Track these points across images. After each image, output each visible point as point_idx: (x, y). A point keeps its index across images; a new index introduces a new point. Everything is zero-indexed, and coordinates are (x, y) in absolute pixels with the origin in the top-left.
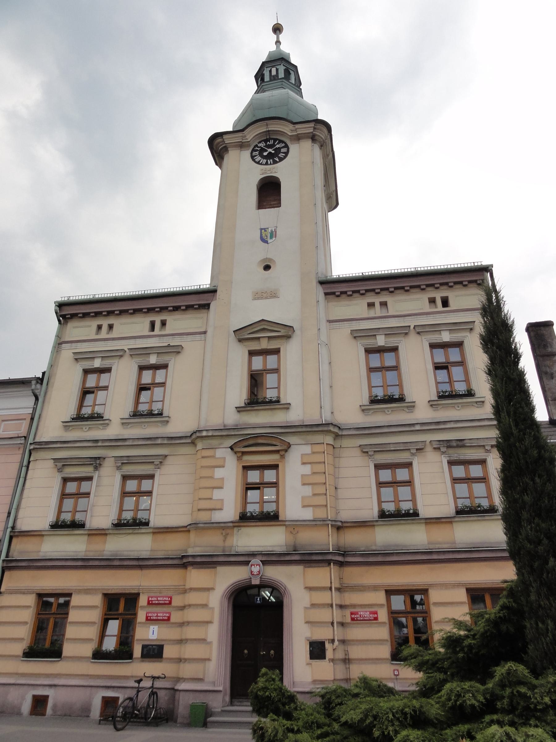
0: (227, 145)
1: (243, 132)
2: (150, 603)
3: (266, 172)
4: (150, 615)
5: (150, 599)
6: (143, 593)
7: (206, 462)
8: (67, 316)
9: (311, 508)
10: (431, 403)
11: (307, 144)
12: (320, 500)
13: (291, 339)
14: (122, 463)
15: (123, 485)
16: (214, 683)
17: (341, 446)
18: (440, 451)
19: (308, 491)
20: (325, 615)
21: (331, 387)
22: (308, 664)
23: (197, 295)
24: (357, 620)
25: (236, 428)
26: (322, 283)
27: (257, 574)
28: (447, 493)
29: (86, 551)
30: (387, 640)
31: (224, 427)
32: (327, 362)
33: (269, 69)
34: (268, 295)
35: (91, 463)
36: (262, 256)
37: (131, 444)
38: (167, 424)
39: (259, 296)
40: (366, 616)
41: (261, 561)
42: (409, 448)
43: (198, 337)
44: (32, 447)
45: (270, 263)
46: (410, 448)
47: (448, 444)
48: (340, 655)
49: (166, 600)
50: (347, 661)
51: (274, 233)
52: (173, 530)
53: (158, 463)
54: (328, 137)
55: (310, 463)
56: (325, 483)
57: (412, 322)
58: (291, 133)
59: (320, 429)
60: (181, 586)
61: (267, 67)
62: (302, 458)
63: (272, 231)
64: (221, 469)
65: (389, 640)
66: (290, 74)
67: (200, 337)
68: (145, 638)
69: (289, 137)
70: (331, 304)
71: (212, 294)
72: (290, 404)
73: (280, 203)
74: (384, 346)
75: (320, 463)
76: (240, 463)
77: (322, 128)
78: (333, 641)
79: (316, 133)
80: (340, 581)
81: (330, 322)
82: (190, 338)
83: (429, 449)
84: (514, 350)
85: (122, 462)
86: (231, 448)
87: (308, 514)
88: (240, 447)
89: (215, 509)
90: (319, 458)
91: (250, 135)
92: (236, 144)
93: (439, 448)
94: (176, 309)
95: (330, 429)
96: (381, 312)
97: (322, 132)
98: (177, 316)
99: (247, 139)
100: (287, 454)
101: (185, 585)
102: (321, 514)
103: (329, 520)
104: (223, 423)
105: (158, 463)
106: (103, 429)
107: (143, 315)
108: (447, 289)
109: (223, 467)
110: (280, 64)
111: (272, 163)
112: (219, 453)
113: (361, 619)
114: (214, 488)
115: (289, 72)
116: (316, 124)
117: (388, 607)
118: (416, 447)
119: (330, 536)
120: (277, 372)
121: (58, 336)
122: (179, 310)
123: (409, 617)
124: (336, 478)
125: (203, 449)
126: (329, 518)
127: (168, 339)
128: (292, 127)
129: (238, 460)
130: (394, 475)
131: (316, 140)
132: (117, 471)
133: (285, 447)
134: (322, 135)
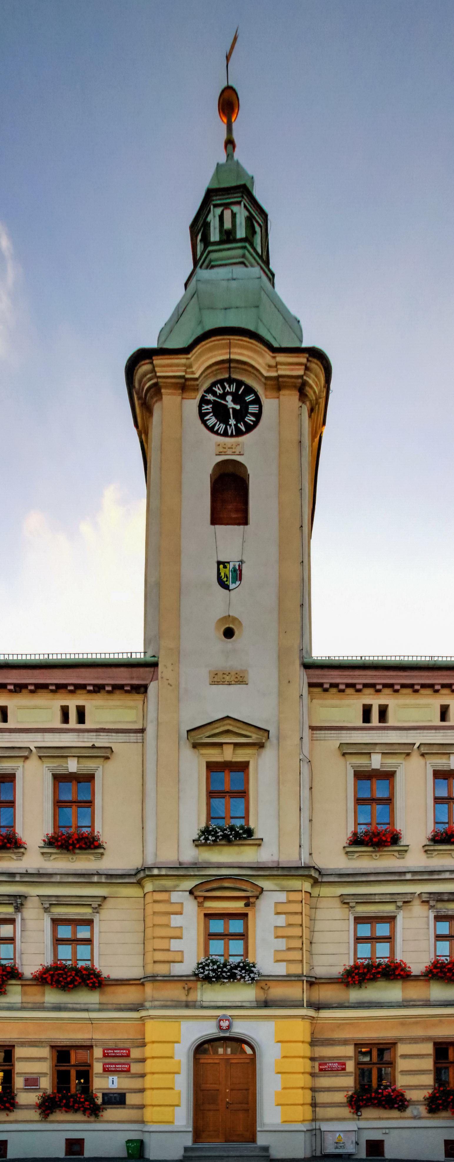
1: (189, 356)
2: (105, 1056)
3: (225, 450)
4: (107, 1066)
5: (106, 1051)
7: (159, 908)
9: (285, 964)
10: (427, 848)
14: (51, 904)
15: (54, 931)
17: (319, 895)
19: (282, 944)
21: (311, 820)
23: (130, 670)
24: (325, 1070)
25: (196, 866)
27: (227, 1029)
31: (180, 865)
32: (307, 787)
33: (218, 211)
34: (232, 679)
35: (10, 902)
36: (219, 613)
40: (334, 1067)
42: (396, 900)
43: (133, 737)
45: (233, 624)
46: (397, 900)
47: (439, 898)
49: (118, 1053)
51: (238, 572)
52: (124, 983)
53: (97, 906)
54: (323, 392)
55: (285, 913)
56: (301, 937)
57: (418, 738)
58: (268, 371)
59: (301, 872)
60: (138, 1039)
61: (216, 206)
62: (275, 907)
63: (234, 568)
64: (178, 917)
67: (135, 738)
68: (105, 1087)
69: (263, 380)
72: (262, 839)
74: (379, 769)
75: (296, 913)
76: (201, 910)
79: (308, 379)
82: (122, 737)
83: (416, 902)
84: (206, 834)
85: (51, 902)
86: (191, 892)
87: (281, 969)
89: (174, 962)
90: (296, 908)
92: (173, 380)
93: (428, 902)
94: (98, 689)
95: (311, 874)
96: (234, 753)
100: (258, 902)
101: (144, 1039)
102: (296, 969)
103: (305, 976)
104: (178, 860)
105: (97, 906)
106: (17, 860)
110: (239, 203)
111: (234, 433)
112: (175, 897)
113: (329, 1069)
116: (310, 359)
118: (404, 900)
120: (242, 797)
122: (102, 691)
123: (375, 1068)
126: (305, 974)
127: (90, 737)
129: (198, 906)
132: (45, 914)
133: (256, 893)
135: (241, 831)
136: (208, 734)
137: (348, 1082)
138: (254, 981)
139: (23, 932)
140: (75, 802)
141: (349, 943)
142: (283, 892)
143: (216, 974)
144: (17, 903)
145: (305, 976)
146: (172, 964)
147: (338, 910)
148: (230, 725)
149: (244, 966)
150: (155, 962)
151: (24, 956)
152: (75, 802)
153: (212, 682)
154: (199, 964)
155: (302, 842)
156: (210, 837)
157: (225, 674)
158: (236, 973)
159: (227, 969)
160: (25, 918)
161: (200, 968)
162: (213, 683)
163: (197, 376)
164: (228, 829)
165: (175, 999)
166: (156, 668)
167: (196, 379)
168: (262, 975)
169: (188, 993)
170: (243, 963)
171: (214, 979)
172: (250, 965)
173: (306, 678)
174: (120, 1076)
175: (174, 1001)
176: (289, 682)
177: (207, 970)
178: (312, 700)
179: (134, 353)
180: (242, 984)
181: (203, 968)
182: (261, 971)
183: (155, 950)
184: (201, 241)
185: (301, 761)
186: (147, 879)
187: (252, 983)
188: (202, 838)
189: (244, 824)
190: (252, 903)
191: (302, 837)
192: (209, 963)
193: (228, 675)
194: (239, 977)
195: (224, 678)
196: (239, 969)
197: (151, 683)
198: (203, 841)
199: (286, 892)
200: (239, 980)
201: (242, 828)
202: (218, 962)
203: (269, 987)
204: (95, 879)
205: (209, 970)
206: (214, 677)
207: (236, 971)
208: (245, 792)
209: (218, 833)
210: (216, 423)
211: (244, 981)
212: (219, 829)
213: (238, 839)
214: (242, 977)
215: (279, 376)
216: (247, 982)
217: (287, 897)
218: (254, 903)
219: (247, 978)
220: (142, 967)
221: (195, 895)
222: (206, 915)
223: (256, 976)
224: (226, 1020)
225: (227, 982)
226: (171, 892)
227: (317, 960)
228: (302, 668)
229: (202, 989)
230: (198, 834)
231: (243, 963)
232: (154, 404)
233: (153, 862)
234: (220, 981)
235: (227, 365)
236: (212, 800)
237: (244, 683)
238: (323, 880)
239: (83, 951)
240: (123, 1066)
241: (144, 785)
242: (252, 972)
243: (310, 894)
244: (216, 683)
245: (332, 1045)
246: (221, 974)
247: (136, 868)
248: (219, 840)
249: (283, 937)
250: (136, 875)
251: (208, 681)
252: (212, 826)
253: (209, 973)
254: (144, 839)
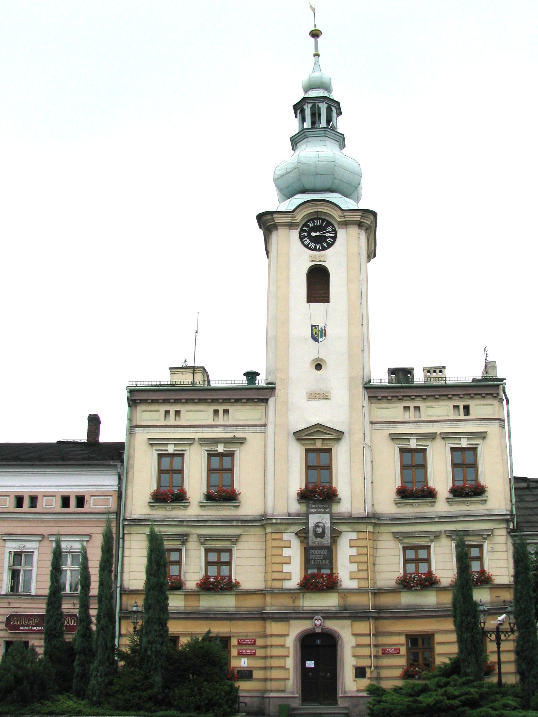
0: (276, 223)
1: (293, 214)
2: (239, 643)
4: (241, 651)
5: (240, 641)
6: (233, 637)
7: (276, 543)
8: (137, 401)
9: (356, 580)
11: (354, 231)
12: (364, 575)
13: (341, 440)
16: (292, 693)
18: (451, 538)
19: (354, 567)
20: (366, 651)
22: (354, 681)
23: (257, 391)
24: (386, 654)
26: (366, 388)
27: (319, 626)
28: (453, 569)
29: (185, 607)
30: (404, 644)
37: (211, 524)
38: (238, 508)
39: (314, 396)
41: (322, 617)
43: (258, 429)
44: (126, 523)
48: (375, 675)
49: (248, 642)
50: (379, 678)
51: (324, 331)
53: (235, 541)
55: (356, 547)
56: (367, 562)
58: (340, 218)
61: (308, 103)
63: (321, 329)
65: (405, 644)
66: (332, 111)
67: (260, 430)
70: (373, 405)
71: (271, 390)
73: (328, 297)
76: (303, 545)
77: (369, 216)
78: (370, 667)
80: (376, 629)
81: (372, 424)
82: (251, 430)
83: (443, 536)
86: (296, 534)
87: (354, 584)
88: (302, 534)
90: (363, 543)
91: (299, 217)
93: (450, 536)
94: (237, 401)
97: (367, 218)
98: (238, 407)
99: (296, 220)
101: (265, 632)
102: (364, 584)
103: (370, 589)
104: (288, 512)
107: (207, 404)
108: (469, 399)
110: (323, 102)
115: (331, 109)
116: (363, 215)
117: (407, 646)
119: (370, 600)
121: (130, 420)
124: (375, 556)
125: (273, 532)
127: (232, 430)
128: (340, 213)
130: (416, 554)
131: (362, 226)
134: (369, 221)
137: (402, 661)
139: (187, 558)
140: (221, 470)
141: (399, 564)
144: (184, 540)
147: (392, 541)
148: (319, 427)
151: (187, 574)
152: (221, 470)
160: (189, 548)
163: (298, 221)
167: (298, 222)
169: (294, 601)
174: (249, 658)
183: (273, 572)
184: (299, 113)
204: (235, 524)
210: (310, 243)
215: (346, 221)
224: (319, 620)
227: (379, 576)
228: (363, 389)
229: (303, 598)
232: (273, 231)
235: (316, 213)
238: (381, 523)
239: (225, 570)
240: (251, 651)
241: (266, 460)
245: (391, 635)
249: (355, 563)
251: (306, 399)
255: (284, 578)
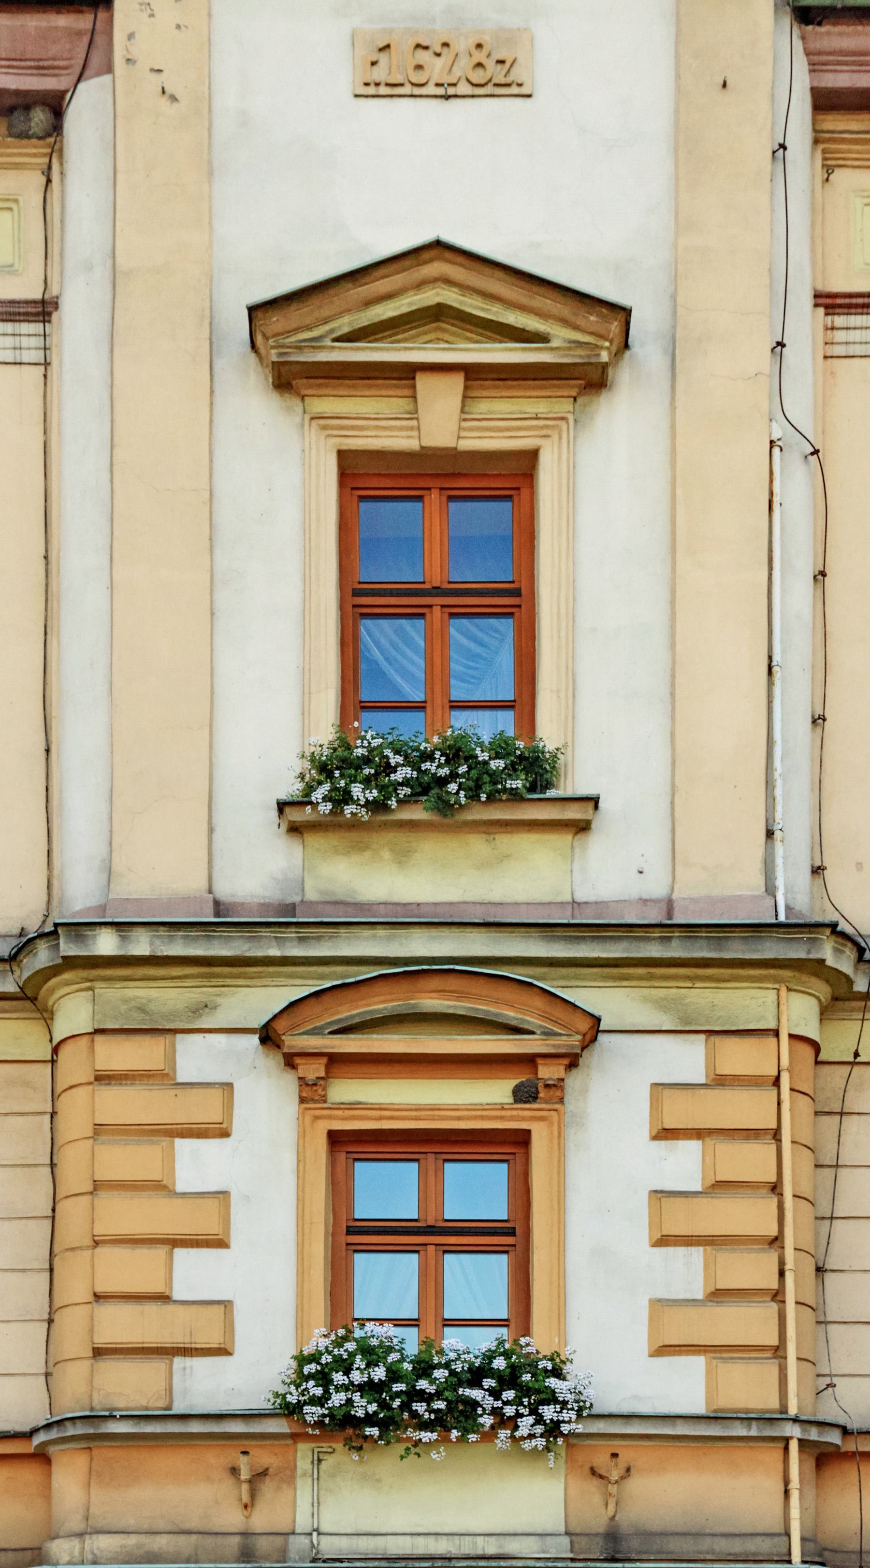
17: (856, 1055)
21: (818, 720)
32: (806, 569)
34: (457, 72)
55: (698, 1134)
56: (776, 1241)
59: (770, 950)
67: (9, 341)
72: (594, 801)
76: (317, 1118)
88: (316, 1032)
100: (574, 1081)
103: (795, 1420)
109: (225, 1134)
114: (175, 1242)
126: (793, 1411)
129: (302, 1100)
135: (497, 764)
136: (345, 324)
138: (560, 1441)
142: (692, 1037)
143: (384, 1405)
145: (795, 1420)
146: (179, 1362)
148: (449, 282)
149: (514, 1370)
150: (98, 1353)
153: (367, 84)
154: (302, 1360)
155: (778, 816)
156: (357, 790)
157: (426, 48)
158: (475, 1404)
159: (433, 1381)
161: (310, 1377)
162: (371, 90)
164: (438, 754)
165: (194, 1523)
166: (102, 15)
168: (594, 1411)
169: (253, 1494)
170: (507, 1355)
171: (375, 1431)
172: (542, 1365)
173: (806, 67)
175: (189, 1532)
176: (724, 85)
177: (338, 1389)
178: (829, 170)
179: (538, 363)
180: (503, 1453)
181: (323, 1378)
182: (590, 1394)
183: (98, 1297)
185: (776, 450)
186: (67, 976)
187: (547, 1449)
188: (318, 794)
189: (511, 733)
190: (547, 1086)
191: (778, 792)
192: (352, 1355)
193: (438, 55)
194: (487, 1421)
195: (419, 67)
196: (488, 1383)
197: (81, 86)
198: (326, 808)
199: (702, 1037)
200: (490, 1435)
201: (501, 748)
202: (390, 1349)
203: (628, 1470)
205: (346, 1388)
206: (373, 64)
207: (476, 1394)
208: (517, 593)
209: (394, 770)
211: (513, 1437)
212: (397, 752)
213: (483, 797)
214: (502, 1421)
216: (527, 1445)
217: (711, 1059)
218: (558, 1085)
219: (526, 1424)
220: (42, 1379)
221: (286, 1050)
222: (336, 1139)
223: (565, 1416)
225: (430, 1444)
226: (179, 1036)
228: (787, 20)
230: (302, 776)
231: (507, 1355)
233: (93, 901)
234: (399, 1440)
236: (367, 627)
237: (514, 90)
242: (552, 1398)
243: (816, 1047)
244: (383, 90)
246: (405, 1406)
247: (16, 931)
248: (399, 802)
249: (688, 1241)
250: (13, 958)
252: (363, 738)
253: (349, 1402)
254: (55, 802)
255: (179, 1338)
